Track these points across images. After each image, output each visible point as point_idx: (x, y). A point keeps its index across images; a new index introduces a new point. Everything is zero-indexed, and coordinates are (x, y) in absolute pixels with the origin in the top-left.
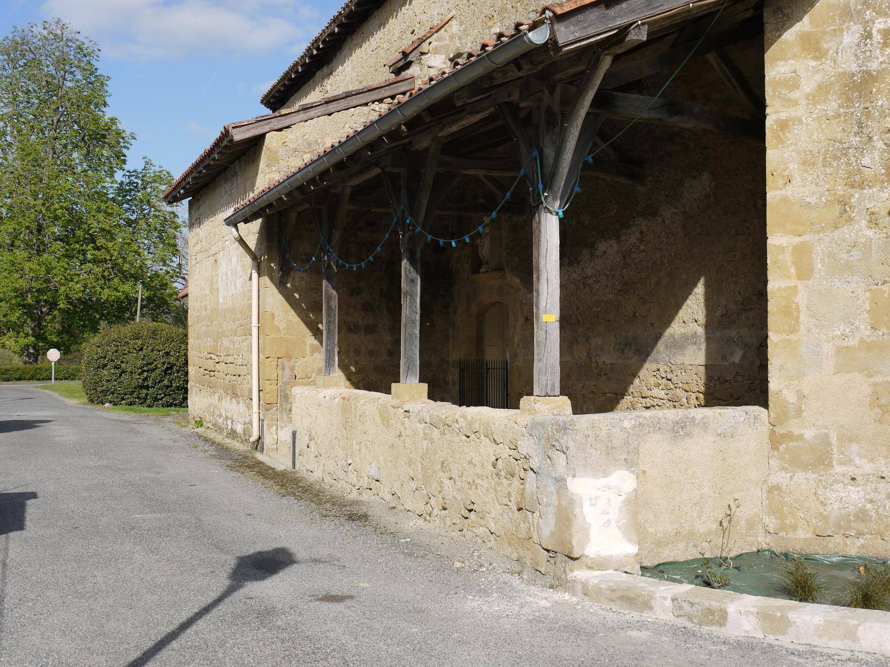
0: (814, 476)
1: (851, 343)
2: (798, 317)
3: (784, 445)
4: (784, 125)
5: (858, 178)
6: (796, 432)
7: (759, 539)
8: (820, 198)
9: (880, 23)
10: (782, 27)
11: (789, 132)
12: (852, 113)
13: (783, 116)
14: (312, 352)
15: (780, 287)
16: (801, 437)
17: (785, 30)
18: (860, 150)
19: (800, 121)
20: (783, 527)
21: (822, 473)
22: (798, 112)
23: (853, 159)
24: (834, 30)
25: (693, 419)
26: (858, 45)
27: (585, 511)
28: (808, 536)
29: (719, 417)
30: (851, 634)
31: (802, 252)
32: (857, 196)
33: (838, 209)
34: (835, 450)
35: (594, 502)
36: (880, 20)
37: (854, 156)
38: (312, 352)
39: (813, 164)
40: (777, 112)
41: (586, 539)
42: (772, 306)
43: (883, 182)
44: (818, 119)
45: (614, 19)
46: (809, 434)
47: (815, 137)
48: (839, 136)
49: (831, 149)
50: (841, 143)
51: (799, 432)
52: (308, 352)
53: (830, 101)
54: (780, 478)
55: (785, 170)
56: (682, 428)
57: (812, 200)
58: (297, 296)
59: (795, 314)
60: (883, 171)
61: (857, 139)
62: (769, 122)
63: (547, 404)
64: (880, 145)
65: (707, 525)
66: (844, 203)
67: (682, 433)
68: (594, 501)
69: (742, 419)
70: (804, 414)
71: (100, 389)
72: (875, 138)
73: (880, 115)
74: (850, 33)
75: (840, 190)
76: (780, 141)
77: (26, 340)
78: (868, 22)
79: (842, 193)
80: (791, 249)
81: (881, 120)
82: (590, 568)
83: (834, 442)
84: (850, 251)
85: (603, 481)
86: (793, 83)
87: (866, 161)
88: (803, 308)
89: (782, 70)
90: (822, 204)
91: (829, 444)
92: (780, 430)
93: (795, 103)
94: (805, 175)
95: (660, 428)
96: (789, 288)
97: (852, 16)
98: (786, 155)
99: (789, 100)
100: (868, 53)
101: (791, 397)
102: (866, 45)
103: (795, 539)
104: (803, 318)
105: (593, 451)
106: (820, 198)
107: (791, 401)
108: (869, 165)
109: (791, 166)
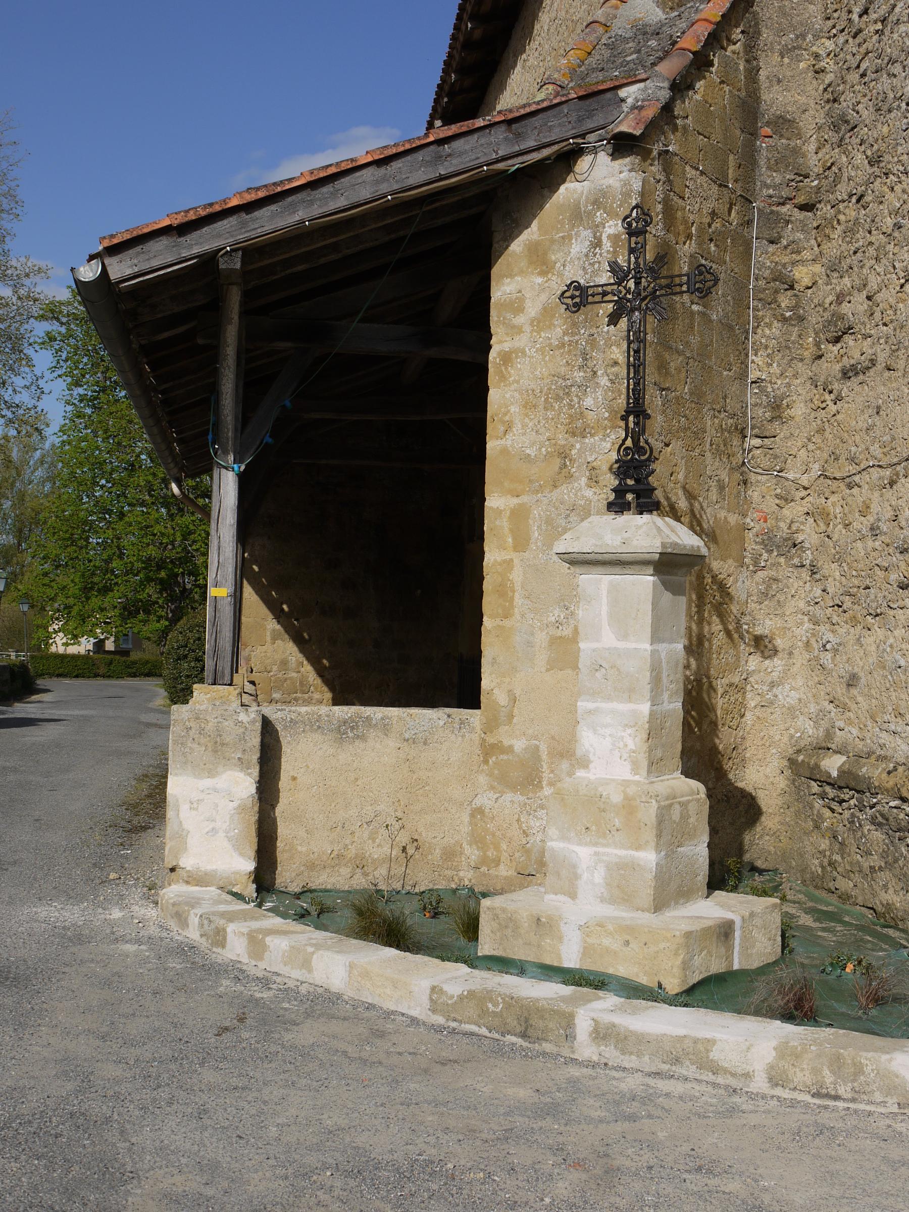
0: (522, 798)
1: (565, 633)
2: (512, 598)
3: (494, 758)
4: (507, 358)
5: (579, 424)
6: (506, 742)
7: (461, 874)
8: (540, 449)
9: (610, 227)
10: (510, 236)
11: (512, 366)
12: (577, 342)
13: (506, 346)
14: (274, 640)
15: (495, 560)
16: (510, 750)
17: (513, 241)
18: (583, 388)
19: (523, 352)
20: (484, 860)
21: (530, 795)
22: (521, 341)
23: (575, 399)
24: (563, 237)
25: (368, 718)
26: (587, 256)
27: (182, 815)
28: (510, 873)
29: (408, 719)
30: (306, 964)
31: (519, 515)
32: (578, 446)
33: (557, 462)
34: (545, 767)
35: (195, 805)
36: (611, 223)
37: (577, 396)
38: (274, 640)
39: (535, 406)
40: (500, 342)
41: (182, 846)
42: (487, 585)
43: (605, 428)
44: (541, 350)
45: (190, 246)
46: (519, 745)
47: (538, 373)
48: (563, 370)
49: (553, 387)
50: (564, 379)
51: (509, 743)
52: (268, 639)
53: (555, 326)
54: (485, 800)
55: (506, 414)
56: (352, 728)
58: (256, 568)
59: (510, 594)
60: (607, 415)
61: (581, 374)
62: (492, 355)
63: (206, 694)
64: (604, 381)
65: (379, 849)
66: (564, 455)
67: (351, 735)
68: (194, 805)
69: (441, 723)
70: (515, 720)
71: (180, 687)
72: (599, 373)
73: (605, 344)
74: (579, 240)
75: (562, 439)
76: (503, 378)
77: (158, 625)
78: (597, 226)
79: (563, 442)
80: (508, 512)
81: (607, 350)
82: (187, 883)
83: (544, 757)
84: (568, 516)
85: (207, 783)
86: (517, 306)
87: (589, 402)
88: (518, 587)
89: (508, 289)
90: (542, 457)
91: (538, 759)
92: (491, 739)
93: (519, 330)
94: (527, 420)
95: (319, 727)
96: (504, 561)
97: (582, 220)
98: (508, 396)
99: (514, 327)
100: (596, 266)
101: (501, 698)
102: (595, 255)
103: (497, 876)
104: (518, 600)
105: (195, 746)
106: (540, 449)
107: (502, 704)
108: (592, 408)
109: (513, 409)
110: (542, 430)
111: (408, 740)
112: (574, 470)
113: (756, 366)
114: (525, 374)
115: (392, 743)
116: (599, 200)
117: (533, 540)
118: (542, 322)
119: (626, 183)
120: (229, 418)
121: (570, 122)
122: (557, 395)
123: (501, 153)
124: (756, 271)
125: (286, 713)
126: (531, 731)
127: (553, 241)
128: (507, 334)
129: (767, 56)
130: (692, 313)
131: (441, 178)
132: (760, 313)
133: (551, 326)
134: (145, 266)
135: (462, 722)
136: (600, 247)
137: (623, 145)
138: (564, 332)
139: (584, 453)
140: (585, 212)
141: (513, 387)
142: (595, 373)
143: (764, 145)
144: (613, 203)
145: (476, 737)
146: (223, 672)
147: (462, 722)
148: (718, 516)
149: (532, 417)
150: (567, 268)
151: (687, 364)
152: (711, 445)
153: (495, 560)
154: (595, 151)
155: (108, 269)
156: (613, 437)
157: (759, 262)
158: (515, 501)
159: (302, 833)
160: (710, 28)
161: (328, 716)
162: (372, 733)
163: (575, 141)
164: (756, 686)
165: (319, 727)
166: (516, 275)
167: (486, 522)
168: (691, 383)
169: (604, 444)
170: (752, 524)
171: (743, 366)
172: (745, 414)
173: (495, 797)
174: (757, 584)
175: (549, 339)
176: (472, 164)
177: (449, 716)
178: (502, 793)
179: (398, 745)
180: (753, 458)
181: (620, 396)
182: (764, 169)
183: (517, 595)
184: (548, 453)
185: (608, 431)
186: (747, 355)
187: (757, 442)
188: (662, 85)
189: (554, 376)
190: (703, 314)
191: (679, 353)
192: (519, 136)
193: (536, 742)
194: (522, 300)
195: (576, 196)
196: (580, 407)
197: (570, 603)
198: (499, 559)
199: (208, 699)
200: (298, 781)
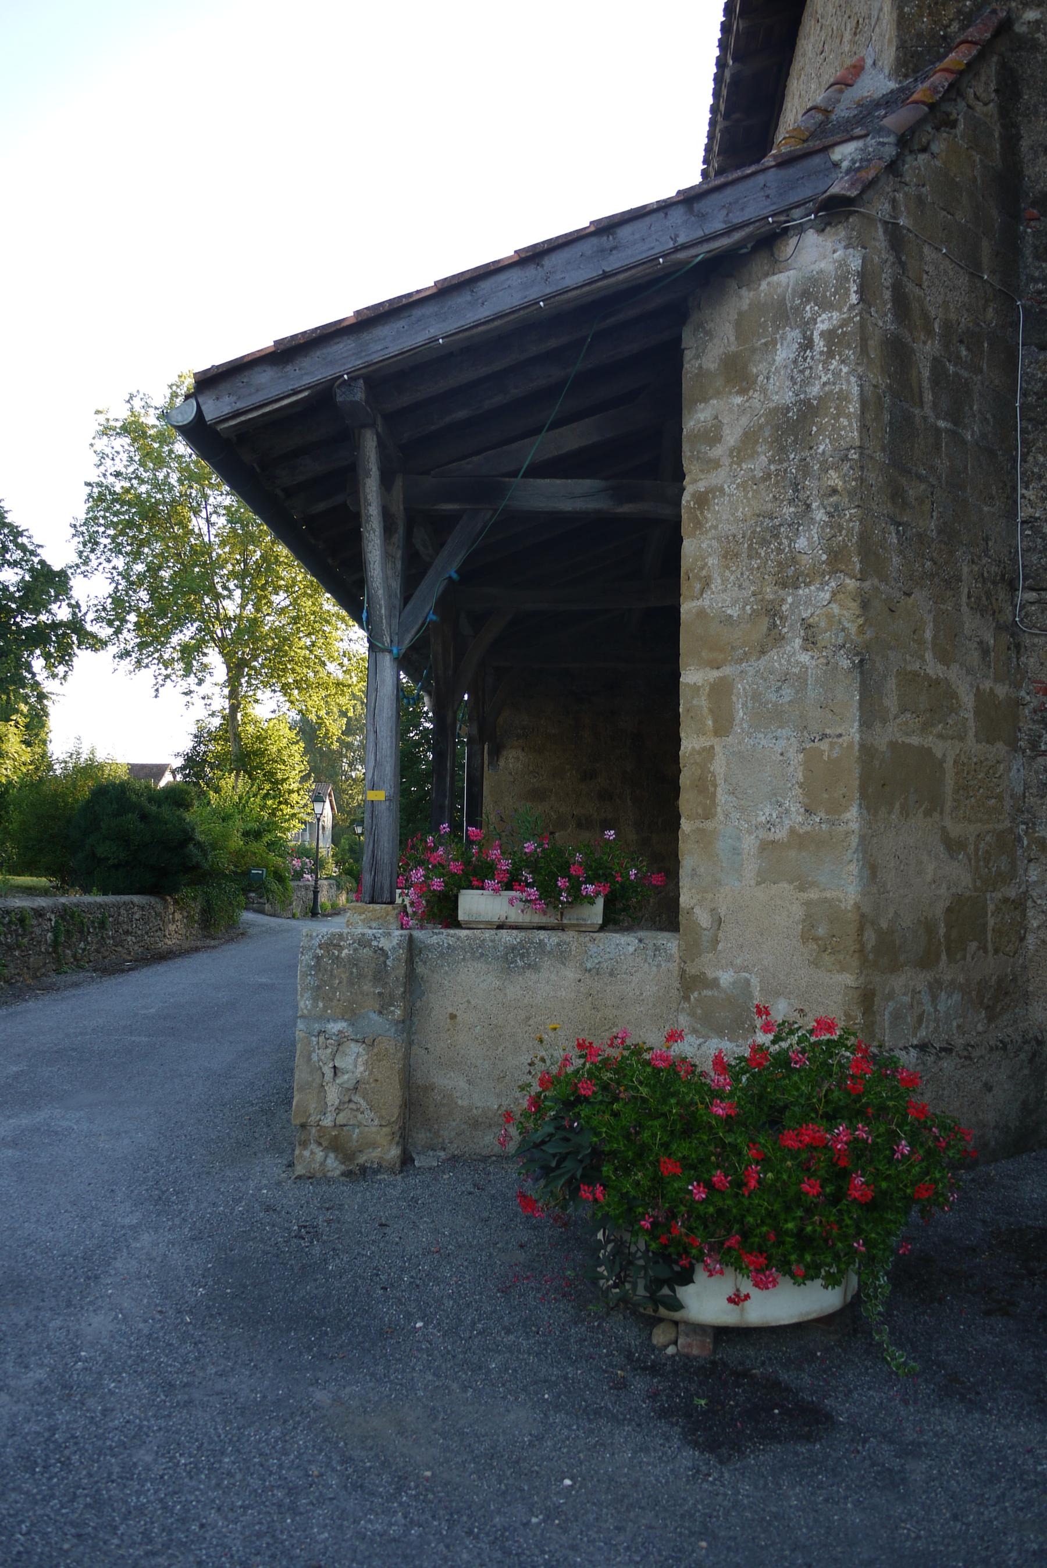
2: (714, 795)
3: (696, 994)
6: (710, 974)
8: (744, 607)
9: (823, 322)
11: (708, 509)
12: (786, 470)
13: (701, 486)
15: (693, 748)
16: (715, 983)
18: (794, 526)
19: (722, 490)
22: (718, 478)
23: (786, 542)
24: (766, 344)
26: (795, 362)
31: (720, 691)
32: (790, 600)
33: (765, 623)
36: (824, 316)
37: (787, 537)
42: (684, 780)
44: (743, 486)
46: (726, 978)
47: (739, 514)
49: (758, 529)
50: (771, 519)
51: (714, 975)
55: (702, 568)
57: (733, 612)
59: (712, 789)
61: (792, 509)
63: (360, 914)
64: (820, 515)
66: (772, 612)
67: (520, 963)
69: (631, 949)
70: (720, 947)
72: (814, 505)
73: (820, 469)
74: (785, 344)
75: (769, 592)
76: (698, 524)
78: (808, 323)
79: (771, 597)
84: (780, 688)
86: (712, 435)
87: (801, 543)
88: (720, 781)
92: (692, 970)
93: (716, 464)
94: (727, 573)
96: (704, 749)
97: (788, 318)
98: (704, 546)
99: (710, 461)
100: (807, 373)
101: (703, 918)
102: (805, 360)
104: (721, 797)
106: (744, 607)
107: (704, 926)
109: (711, 561)
110: (746, 584)
111: (590, 970)
112: (785, 630)
113: (1027, 502)
114: (724, 517)
115: (570, 973)
116: (810, 291)
117: (737, 721)
118: (743, 451)
119: (842, 264)
120: (380, 592)
121: (768, 197)
122: (764, 539)
123: (681, 240)
124: (1025, 385)
125: (442, 937)
126: (739, 961)
127: (753, 351)
128: (702, 471)
129: (1029, 122)
130: (938, 430)
131: (606, 275)
132: (1031, 437)
133: (754, 455)
134: (240, 405)
135: (657, 949)
136: (811, 349)
137: (833, 210)
138: (769, 461)
139: (797, 607)
140: (791, 308)
141: (710, 535)
142: (809, 506)
143: (1029, 230)
144: (825, 291)
145: (674, 967)
146: (382, 888)
147: (657, 949)
148: (981, 687)
149: (734, 568)
150: (771, 381)
151: (932, 494)
152: (969, 597)
153: (693, 748)
154: (801, 229)
155: (203, 408)
156: (833, 584)
157: (1027, 373)
158: (715, 674)
159: (462, 1084)
160: (951, 77)
161: (493, 941)
162: (546, 963)
163: (775, 219)
164: (1039, 902)
165: (482, 955)
166: (711, 398)
167: (681, 702)
168: (938, 519)
169: (822, 594)
170: (1028, 698)
171: (1010, 502)
172: (1015, 561)
173: (698, 1042)
174: (1037, 772)
175: (752, 470)
176: (644, 256)
177: (640, 941)
178: (707, 1038)
179: (578, 976)
180: (1027, 615)
181: (840, 532)
182: (1030, 260)
183: (719, 789)
184: (753, 611)
185: (827, 578)
186: (1014, 489)
187: (1033, 596)
188: (885, 140)
189: (759, 516)
190: (953, 433)
191: (919, 477)
192: (703, 217)
193: (746, 975)
194: (718, 425)
195: (779, 290)
196: (791, 551)
197: (785, 798)
198: (697, 747)
199: (363, 921)
200: (459, 1018)
